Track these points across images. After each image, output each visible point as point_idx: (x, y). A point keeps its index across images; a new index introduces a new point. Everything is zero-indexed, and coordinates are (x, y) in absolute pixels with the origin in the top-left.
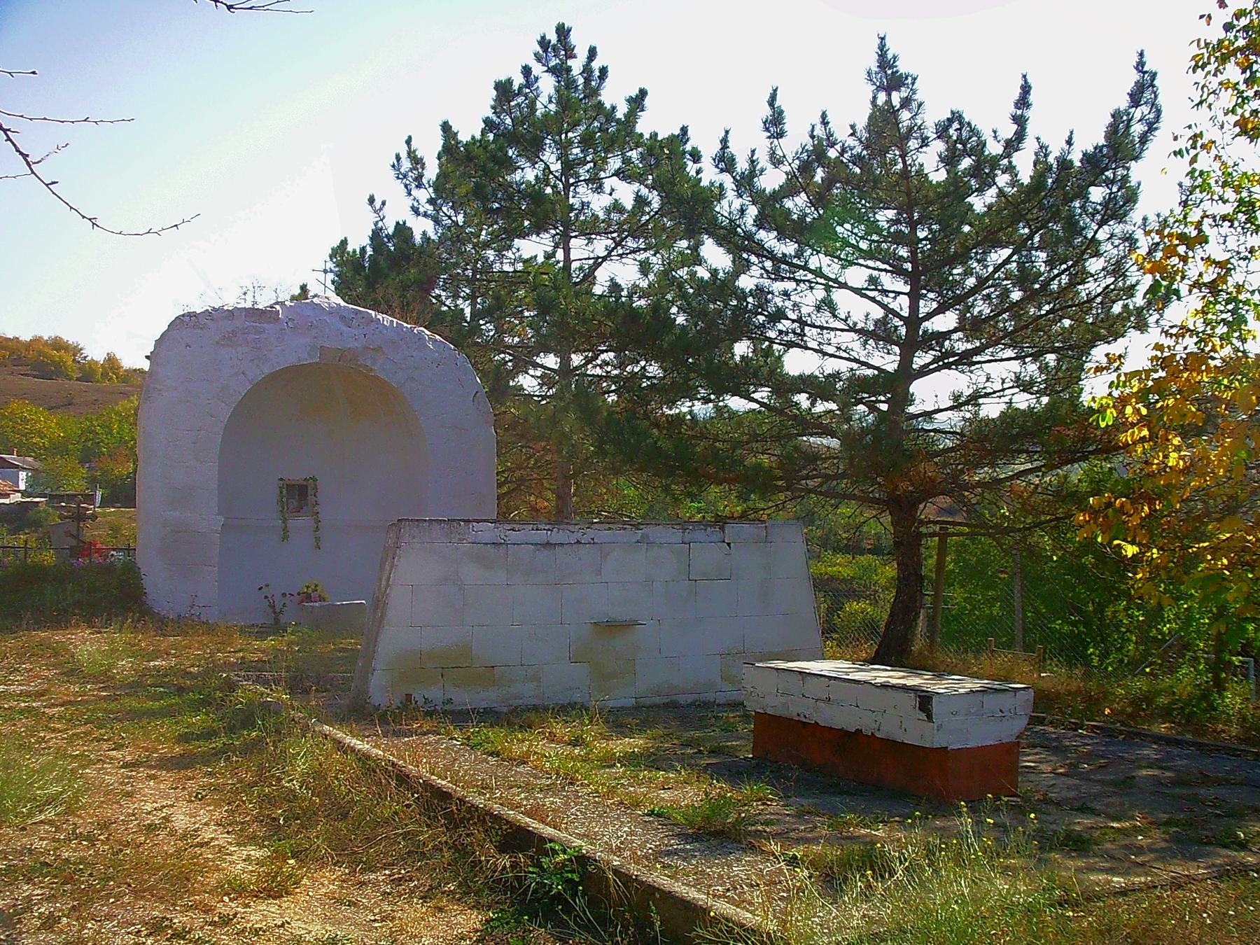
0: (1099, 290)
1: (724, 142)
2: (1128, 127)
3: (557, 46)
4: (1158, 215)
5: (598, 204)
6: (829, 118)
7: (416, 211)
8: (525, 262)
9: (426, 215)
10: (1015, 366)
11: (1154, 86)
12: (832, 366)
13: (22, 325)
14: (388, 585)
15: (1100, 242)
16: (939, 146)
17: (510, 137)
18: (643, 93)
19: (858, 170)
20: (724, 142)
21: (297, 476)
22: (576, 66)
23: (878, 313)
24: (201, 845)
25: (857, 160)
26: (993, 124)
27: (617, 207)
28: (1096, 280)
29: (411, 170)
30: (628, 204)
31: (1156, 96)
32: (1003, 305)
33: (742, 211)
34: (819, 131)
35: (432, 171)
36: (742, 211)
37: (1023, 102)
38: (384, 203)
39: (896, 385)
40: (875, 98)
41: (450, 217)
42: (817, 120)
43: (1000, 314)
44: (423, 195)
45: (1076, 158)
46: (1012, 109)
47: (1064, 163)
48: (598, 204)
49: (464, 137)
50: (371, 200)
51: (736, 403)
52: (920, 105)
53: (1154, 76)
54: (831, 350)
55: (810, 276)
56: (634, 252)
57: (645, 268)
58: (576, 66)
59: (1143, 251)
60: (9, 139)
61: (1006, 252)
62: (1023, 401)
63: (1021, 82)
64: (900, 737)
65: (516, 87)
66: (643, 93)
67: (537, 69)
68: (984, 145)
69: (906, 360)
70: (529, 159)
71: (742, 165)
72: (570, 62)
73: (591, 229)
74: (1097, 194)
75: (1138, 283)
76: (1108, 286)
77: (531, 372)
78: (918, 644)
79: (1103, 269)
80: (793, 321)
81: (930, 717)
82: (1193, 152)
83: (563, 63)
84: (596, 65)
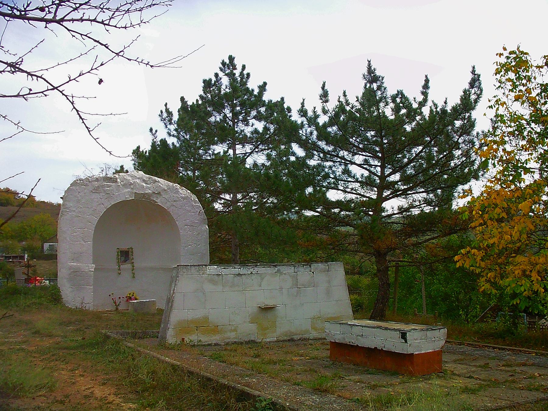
0: (460, 163)
1: (303, 104)
2: (469, 96)
3: (229, 65)
4: (483, 132)
5: (248, 131)
6: (347, 94)
7: (169, 134)
8: (215, 155)
9: (173, 136)
10: (424, 195)
11: (479, 80)
12: (349, 196)
13: (2, 186)
14: (174, 293)
15: (460, 143)
16: (392, 105)
17: (211, 103)
18: (265, 84)
19: (358, 115)
20: (303, 104)
21: (125, 247)
22: (237, 72)
23: (366, 173)
24: (109, 403)
25: (358, 111)
26: (414, 95)
27: (256, 131)
28: (458, 159)
29: (167, 117)
30: (261, 130)
31: (480, 85)
32: (419, 170)
33: (311, 133)
34: (342, 99)
35: (176, 117)
36: (311, 133)
37: (426, 86)
38: (156, 131)
39: (376, 205)
40: (366, 85)
41: (184, 137)
42: (341, 95)
43: (419, 174)
44: (172, 127)
45: (449, 109)
46: (421, 89)
47: (444, 111)
48: (248, 131)
49: (190, 103)
50: (151, 130)
51: (309, 213)
52: (385, 89)
53: (479, 76)
54: (348, 190)
55: (339, 160)
56: (262, 150)
57: (269, 157)
58: (237, 72)
59: (477, 147)
60: (83, 122)
61: (420, 148)
62: (427, 209)
63: (424, 78)
64: (393, 350)
65: (213, 82)
66: (265, 84)
67: (221, 74)
68: (411, 105)
69: (380, 194)
70: (218, 112)
71: (310, 114)
72: (234, 71)
73: (244, 140)
74: (458, 123)
75: (475, 160)
76: (463, 161)
77: (219, 201)
78: (388, 313)
79: (461, 154)
80: (333, 178)
81: (406, 342)
82: (497, 106)
83: (232, 72)
84: (245, 72)
